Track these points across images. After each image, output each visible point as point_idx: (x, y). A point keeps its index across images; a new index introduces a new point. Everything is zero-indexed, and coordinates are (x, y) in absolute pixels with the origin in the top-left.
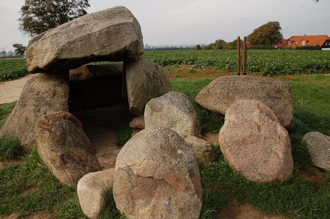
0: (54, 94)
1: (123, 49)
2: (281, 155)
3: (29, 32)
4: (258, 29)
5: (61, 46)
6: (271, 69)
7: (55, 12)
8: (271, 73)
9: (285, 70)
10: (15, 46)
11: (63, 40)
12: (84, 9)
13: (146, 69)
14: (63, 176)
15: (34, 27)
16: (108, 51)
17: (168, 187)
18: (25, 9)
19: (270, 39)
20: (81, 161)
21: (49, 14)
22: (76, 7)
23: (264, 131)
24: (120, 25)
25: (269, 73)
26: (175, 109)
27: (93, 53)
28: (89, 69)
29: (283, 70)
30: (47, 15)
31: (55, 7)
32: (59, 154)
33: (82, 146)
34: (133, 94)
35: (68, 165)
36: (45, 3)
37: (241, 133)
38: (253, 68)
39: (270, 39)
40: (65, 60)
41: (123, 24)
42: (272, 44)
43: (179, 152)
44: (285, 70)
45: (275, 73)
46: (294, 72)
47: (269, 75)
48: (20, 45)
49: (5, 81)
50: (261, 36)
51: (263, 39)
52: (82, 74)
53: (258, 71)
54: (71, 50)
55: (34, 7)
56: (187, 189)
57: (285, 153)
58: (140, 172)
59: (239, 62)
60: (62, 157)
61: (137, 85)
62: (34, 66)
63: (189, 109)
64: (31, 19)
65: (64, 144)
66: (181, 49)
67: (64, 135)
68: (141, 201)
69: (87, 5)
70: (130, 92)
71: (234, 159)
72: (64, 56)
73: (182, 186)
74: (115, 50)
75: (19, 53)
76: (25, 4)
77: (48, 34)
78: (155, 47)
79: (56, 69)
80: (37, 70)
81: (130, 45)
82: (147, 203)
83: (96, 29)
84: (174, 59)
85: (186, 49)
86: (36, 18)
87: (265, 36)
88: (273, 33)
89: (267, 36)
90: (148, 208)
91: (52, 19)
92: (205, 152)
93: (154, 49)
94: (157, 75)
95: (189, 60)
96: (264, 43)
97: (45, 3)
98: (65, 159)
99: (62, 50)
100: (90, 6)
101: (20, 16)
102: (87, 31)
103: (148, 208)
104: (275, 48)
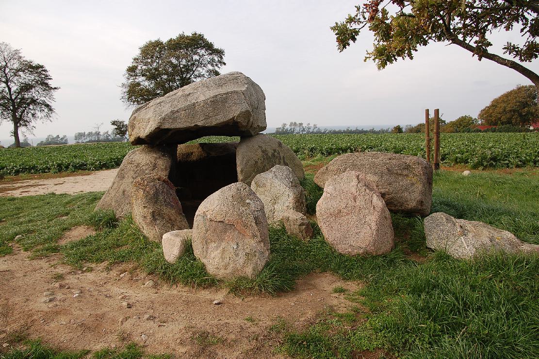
0: (155, 166)
1: (231, 119)
2: (374, 227)
3: (136, 103)
4: (500, 98)
5: (163, 115)
6: (484, 158)
7: (172, 75)
8: (485, 164)
9: (509, 161)
10: (114, 123)
11: (167, 109)
12: (217, 68)
13: (263, 145)
14: (149, 232)
15: (141, 95)
16: (214, 121)
17: (236, 232)
18: (132, 70)
19: (520, 115)
20: (170, 220)
21: (165, 77)
22: (204, 66)
23: (360, 202)
24: (227, 93)
25: (482, 165)
26: (277, 182)
27: (197, 123)
28: (202, 148)
29: (506, 160)
30: (162, 78)
31: (175, 67)
32: (151, 211)
33: (172, 206)
34: (242, 171)
35: (158, 222)
36: (160, 61)
37: (335, 205)
38: (457, 158)
39: (520, 115)
40: (168, 130)
41: (232, 93)
42: (524, 123)
43: (248, 201)
44: (509, 161)
45: (491, 165)
46: (524, 163)
47: (481, 168)
48: (121, 123)
49: (97, 170)
50: (505, 110)
51: (508, 115)
52: (192, 153)
53: (466, 162)
54: (175, 119)
55: (144, 67)
56: (254, 236)
57: (380, 225)
58: (213, 217)
59: (429, 147)
60: (153, 214)
61: (248, 161)
62: (135, 136)
63: (292, 182)
64: (139, 84)
65: (156, 202)
66: (373, 132)
67: (156, 194)
68: (213, 245)
69: (220, 62)
70: (239, 169)
71: (329, 233)
72: (167, 126)
73: (249, 233)
74: (222, 120)
75: (119, 134)
76: (132, 63)
77: (152, 102)
78: (329, 129)
79: (161, 140)
80: (138, 141)
81: (238, 116)
82: (217, 247)
83: (202, 98)
84: (344, 146)
85: (378, 132)
86: (147, 83)
87: (511, 111)
88: (525, 105)
89: (514, 111)
90: (219, 251)
91: (169, 84)
92: (300, 225)
93: (327, 132)
94: (279, 153)
95: (367, 147)
96: (509, 122)
97: (160, 61)
98: (155, 216)
99: (164, 119)
100: (225, 64)
101: (125, 81)
102: (192, 100)
103: (219, 251)
104: (528, 131)
